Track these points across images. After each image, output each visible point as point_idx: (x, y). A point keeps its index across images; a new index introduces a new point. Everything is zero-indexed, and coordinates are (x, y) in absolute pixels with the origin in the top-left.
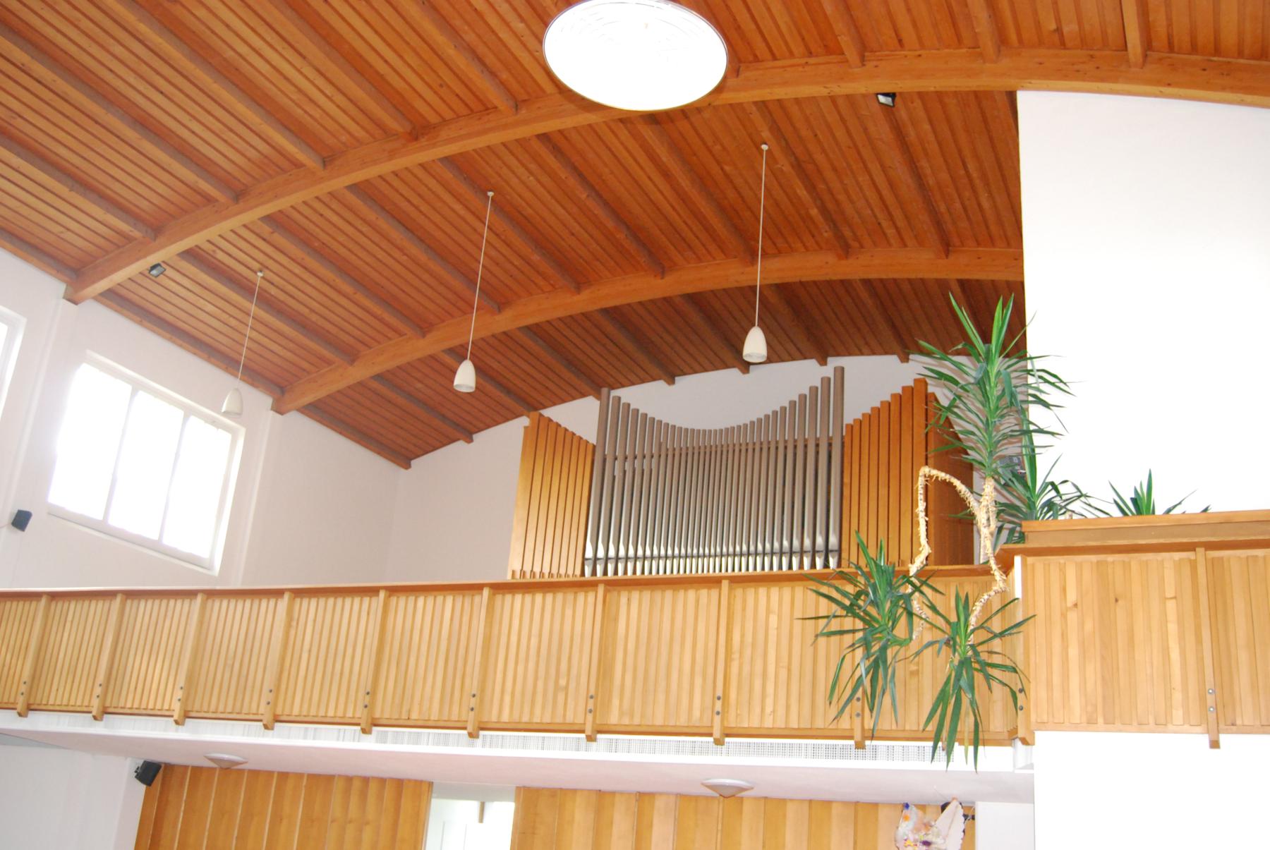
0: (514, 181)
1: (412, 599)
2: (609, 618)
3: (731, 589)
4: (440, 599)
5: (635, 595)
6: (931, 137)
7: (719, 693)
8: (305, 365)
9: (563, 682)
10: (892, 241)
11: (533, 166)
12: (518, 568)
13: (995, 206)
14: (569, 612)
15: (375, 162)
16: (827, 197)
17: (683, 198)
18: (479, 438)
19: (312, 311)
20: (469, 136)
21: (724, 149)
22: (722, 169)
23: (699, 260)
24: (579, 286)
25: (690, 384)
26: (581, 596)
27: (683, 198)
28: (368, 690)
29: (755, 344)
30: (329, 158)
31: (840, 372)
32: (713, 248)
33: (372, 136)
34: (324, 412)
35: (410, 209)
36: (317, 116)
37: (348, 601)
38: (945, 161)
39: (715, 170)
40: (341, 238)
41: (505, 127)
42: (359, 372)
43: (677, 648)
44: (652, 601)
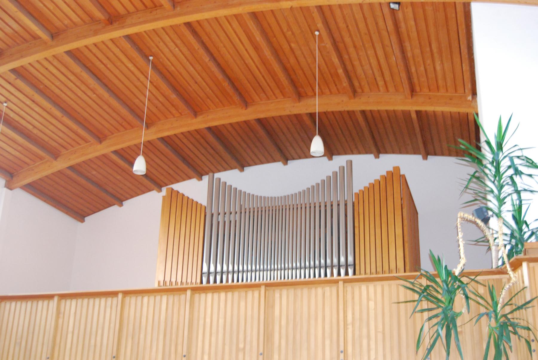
0: (166, 50)
1: (139, 298)
2: (269, 306)
3: (124, 297)
4: (158, 298)
5: (284, 292)
6: (414, 29)
7: (342, 348)
8: (27, 160)
9: (241, 346)
10: (381, 89)
11: (178, 42)
12: (162, 280)
13: (443, 69)
14: (243, 304)
15: (85, 37)
16: (348, 63)
17: (264, 62)
18: (126, 203)
19: (34, 127)
20: (145, 22)
21: (293, 33)
22: (290, 46)
23: (268, 99)
24: (196, 114)
25: (252, 171)
26: (250, 294)
27: (264, 62)
28: (114, 355)
29: (317, 145)
30: (56, 34)
31: (350, 163)
32: (277, 92)
33: (84, 22)
34: (37, 189)
35: (101, 67)
36: (51, 8)
37: (97, 300)
38: (420, 43)
39: (286, 46)
40: (58, 83)
41: (168, 17)
42: (60, 165)
43: (313, 322)
44: (295, 295)
